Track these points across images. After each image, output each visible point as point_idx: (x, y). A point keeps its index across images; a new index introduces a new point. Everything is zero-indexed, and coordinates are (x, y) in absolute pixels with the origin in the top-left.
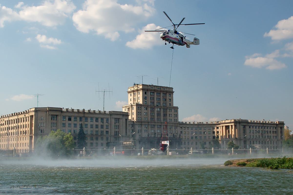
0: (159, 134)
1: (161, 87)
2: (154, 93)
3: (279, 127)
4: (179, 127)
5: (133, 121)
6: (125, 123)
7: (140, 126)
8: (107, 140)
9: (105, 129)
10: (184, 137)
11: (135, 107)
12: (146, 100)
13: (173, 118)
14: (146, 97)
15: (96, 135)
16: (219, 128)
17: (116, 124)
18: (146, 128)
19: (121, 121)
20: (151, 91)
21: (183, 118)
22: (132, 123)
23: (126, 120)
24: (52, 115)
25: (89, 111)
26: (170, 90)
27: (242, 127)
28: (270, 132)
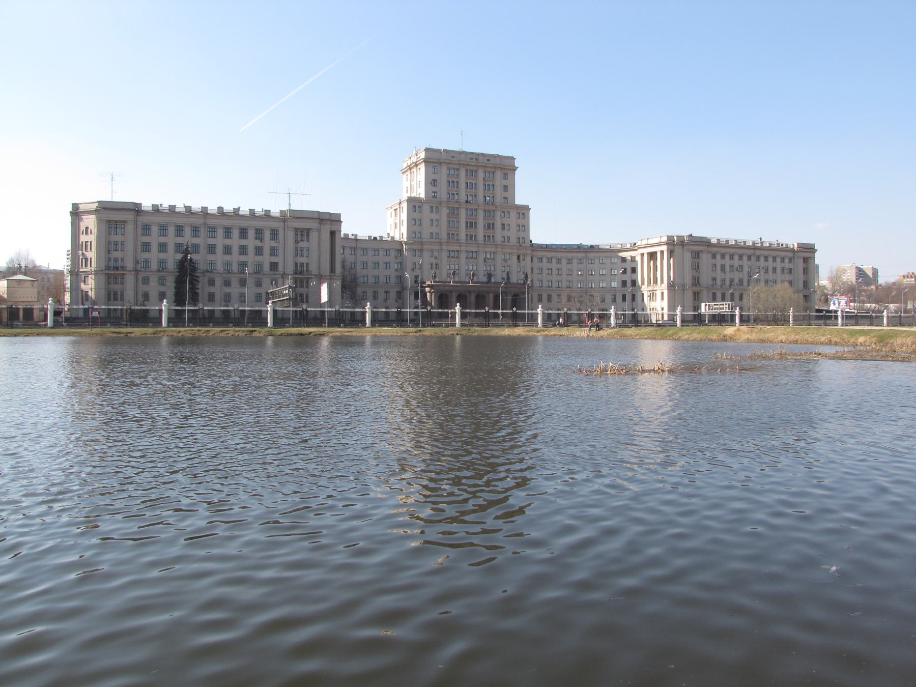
2: (458, 169)
3: (799, 257)
9: (266, 259)
10: (536, 284)
12: (434, 189)
13: (513, 234)
14: (435, 181)
17: (301, 244)
18: (436, 258)
19: (314, 236)
20: (451, 166)
21: (541, 232)
24: (109, 221)
25: (220, 209)
27: (688, 256)
28: (774, 269)
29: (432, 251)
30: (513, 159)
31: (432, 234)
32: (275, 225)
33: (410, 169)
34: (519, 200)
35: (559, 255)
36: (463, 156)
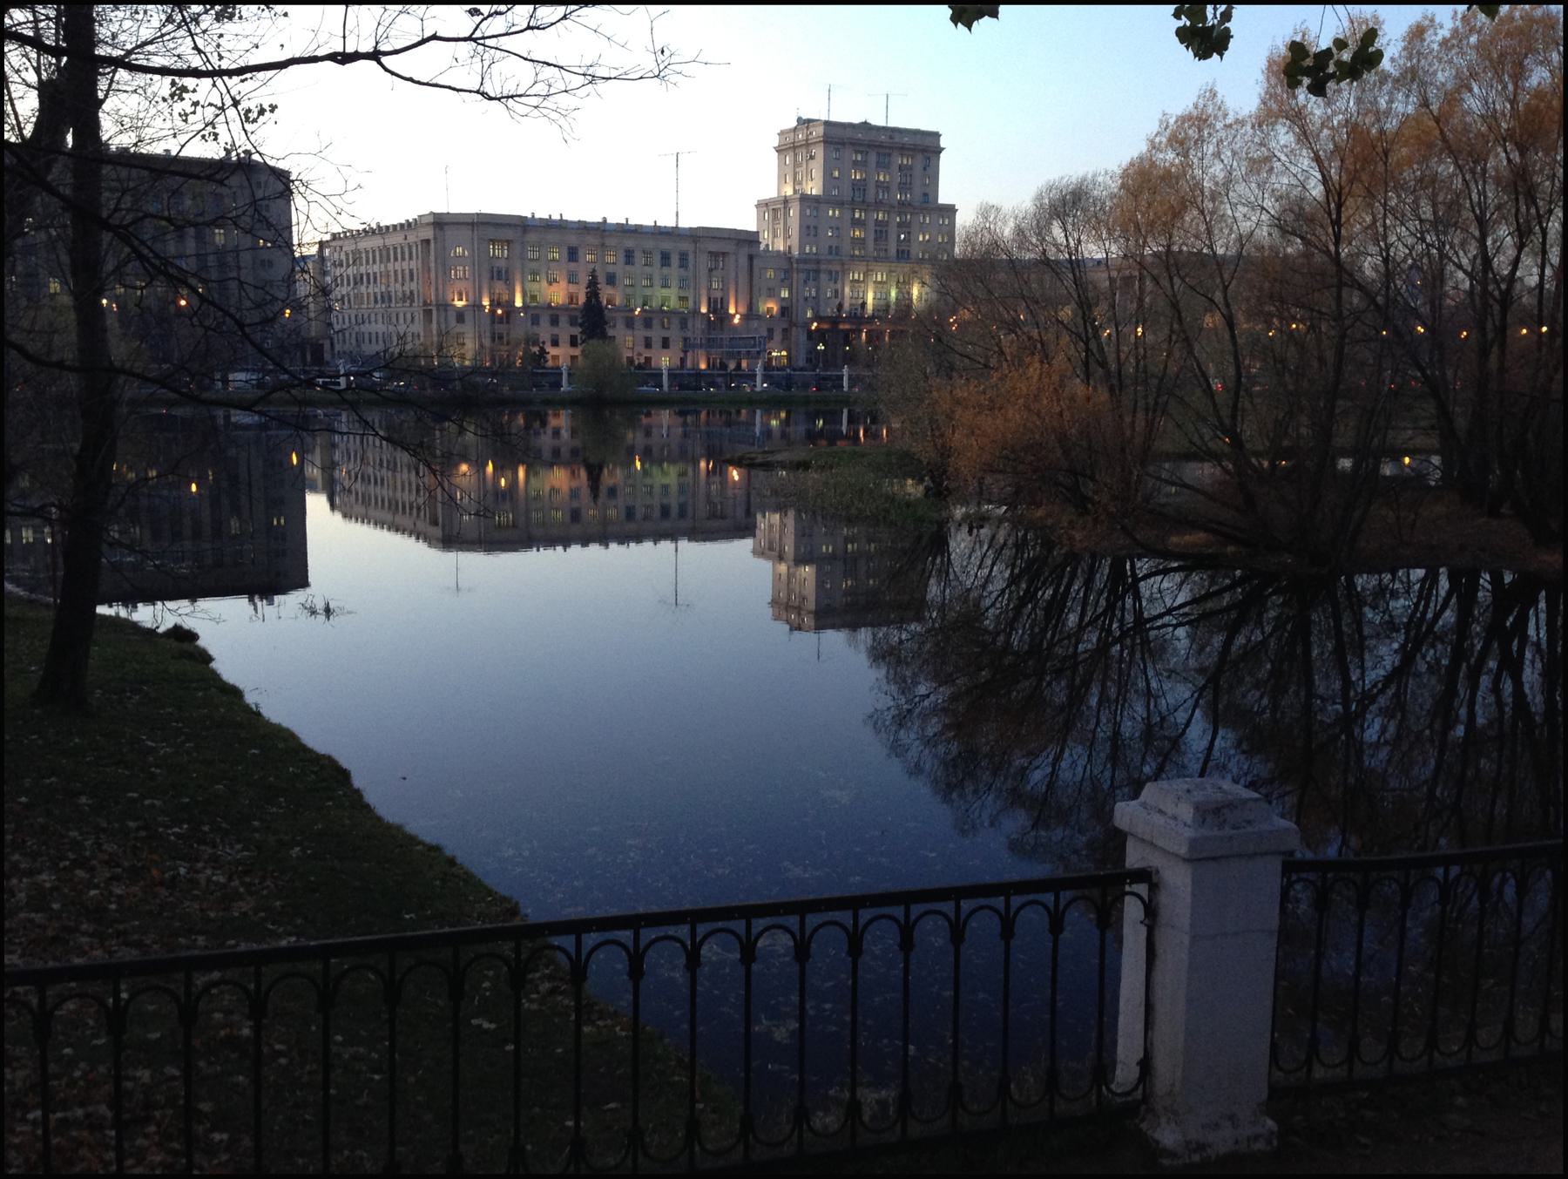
11: (794, 212)
23: (751, 258)
26: (928, 142)
30: (937, 135)
32: (686, 246)
34: (943, 199)
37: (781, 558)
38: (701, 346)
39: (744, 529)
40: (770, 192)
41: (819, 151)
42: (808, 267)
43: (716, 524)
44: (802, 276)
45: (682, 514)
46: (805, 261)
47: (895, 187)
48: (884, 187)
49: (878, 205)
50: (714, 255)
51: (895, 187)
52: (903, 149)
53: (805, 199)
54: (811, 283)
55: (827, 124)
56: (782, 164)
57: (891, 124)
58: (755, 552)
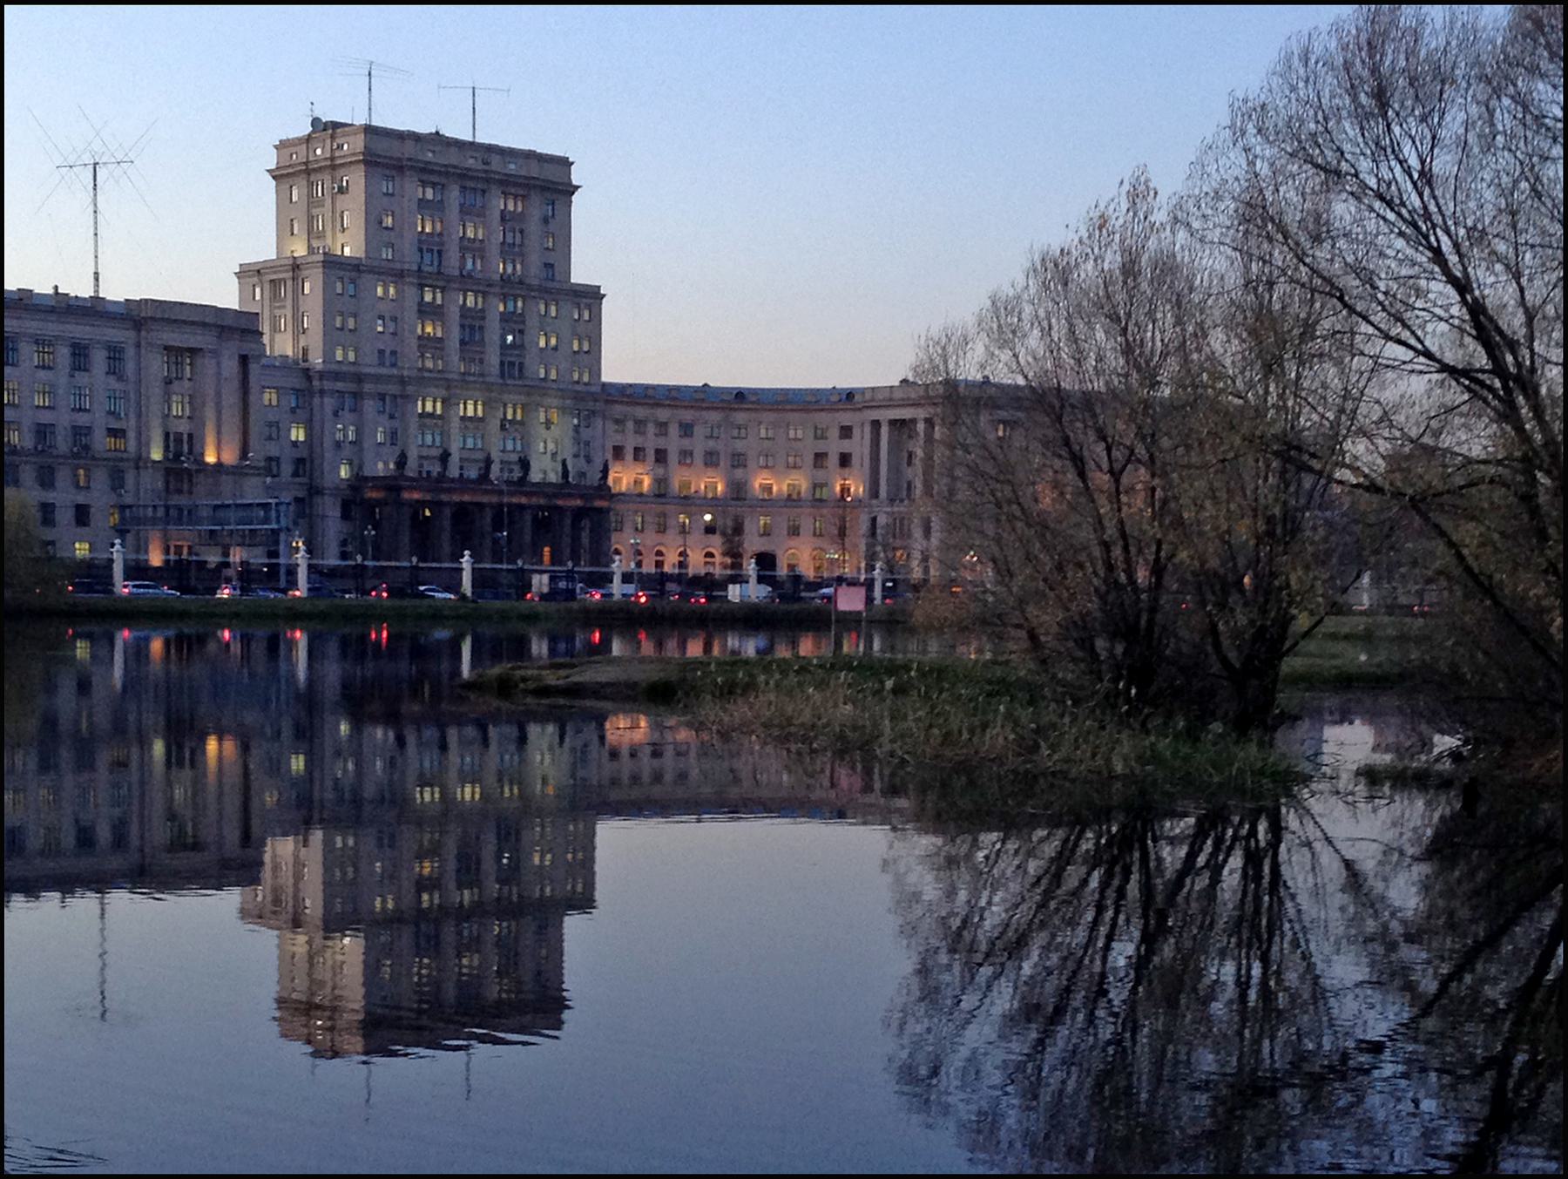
0: (476, 461)
1: (491, 149)
4: (604, 418)
5: (1147, 404)
6: (236, 384)
7: (348, 402)
8: (114, 489)
11: (312, 287)
15: (37, 452)
16: (856, 432)
21: (629, 355)
22: (297, 382)
23: (244, 360)
26: (550, 173)
29: (382, 397)
30: (565, 163)
31: (381, 352)
32: (115, 334)
33: (308, 172)
34: (580, 275)
35: (663, 414)
36: (409, 144)
37: (296, 923)
38: (154, 521)
39: (237, 867)
40: (264, 250)
41: (356, 179)
42: (340, 385)
43: (183, 860)
44: (329, 403)
45: (120, 841)
46: (337, 376)
47: (494, 250)
48: (468, 247)
49: (466, 281)
50: (174, 353)
51: (494, 250)
52: (509, 184)
53: (332, 263)
54: (347, 415)
55: (369, 130)
56: (284, 202)
57: (483, 138)
58: (244, 914)
